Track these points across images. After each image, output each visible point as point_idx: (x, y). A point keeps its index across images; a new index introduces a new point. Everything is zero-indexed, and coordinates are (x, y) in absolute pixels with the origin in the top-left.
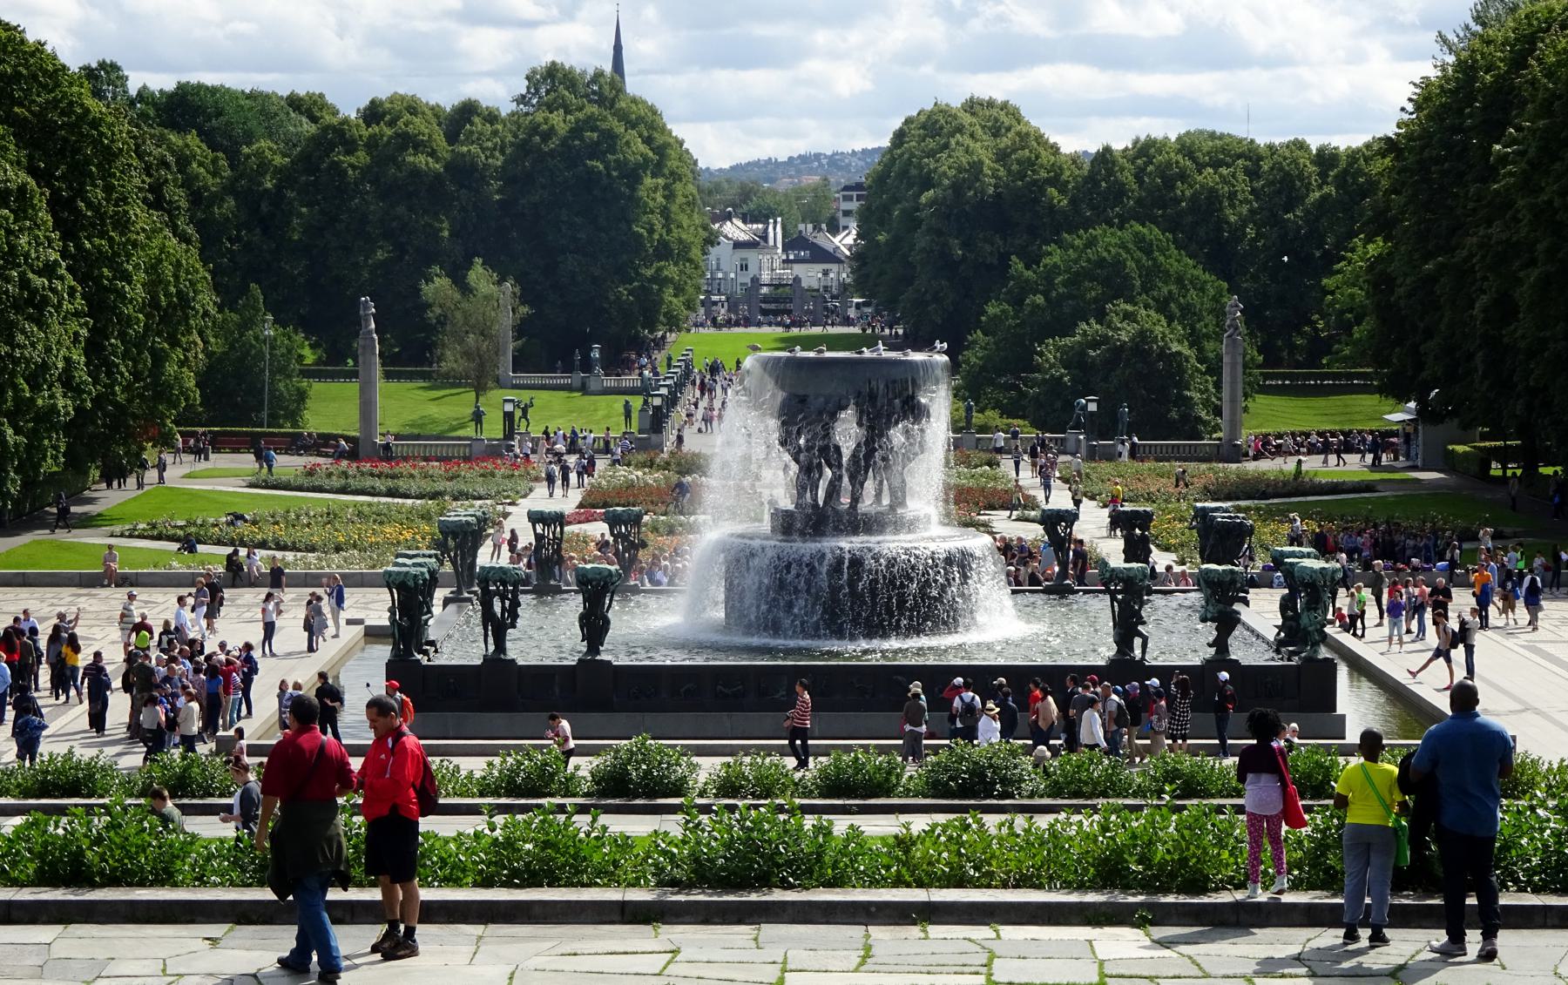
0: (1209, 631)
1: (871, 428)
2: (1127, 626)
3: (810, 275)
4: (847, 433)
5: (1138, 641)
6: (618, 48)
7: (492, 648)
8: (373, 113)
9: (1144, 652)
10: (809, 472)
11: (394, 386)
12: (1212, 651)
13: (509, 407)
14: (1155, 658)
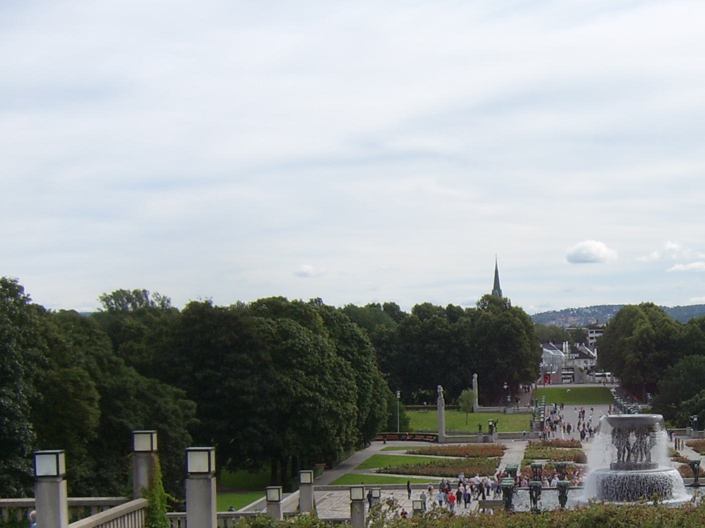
6: (496, 272)
8: (417, 309)
11: (449, 412)
13: (491, 423)
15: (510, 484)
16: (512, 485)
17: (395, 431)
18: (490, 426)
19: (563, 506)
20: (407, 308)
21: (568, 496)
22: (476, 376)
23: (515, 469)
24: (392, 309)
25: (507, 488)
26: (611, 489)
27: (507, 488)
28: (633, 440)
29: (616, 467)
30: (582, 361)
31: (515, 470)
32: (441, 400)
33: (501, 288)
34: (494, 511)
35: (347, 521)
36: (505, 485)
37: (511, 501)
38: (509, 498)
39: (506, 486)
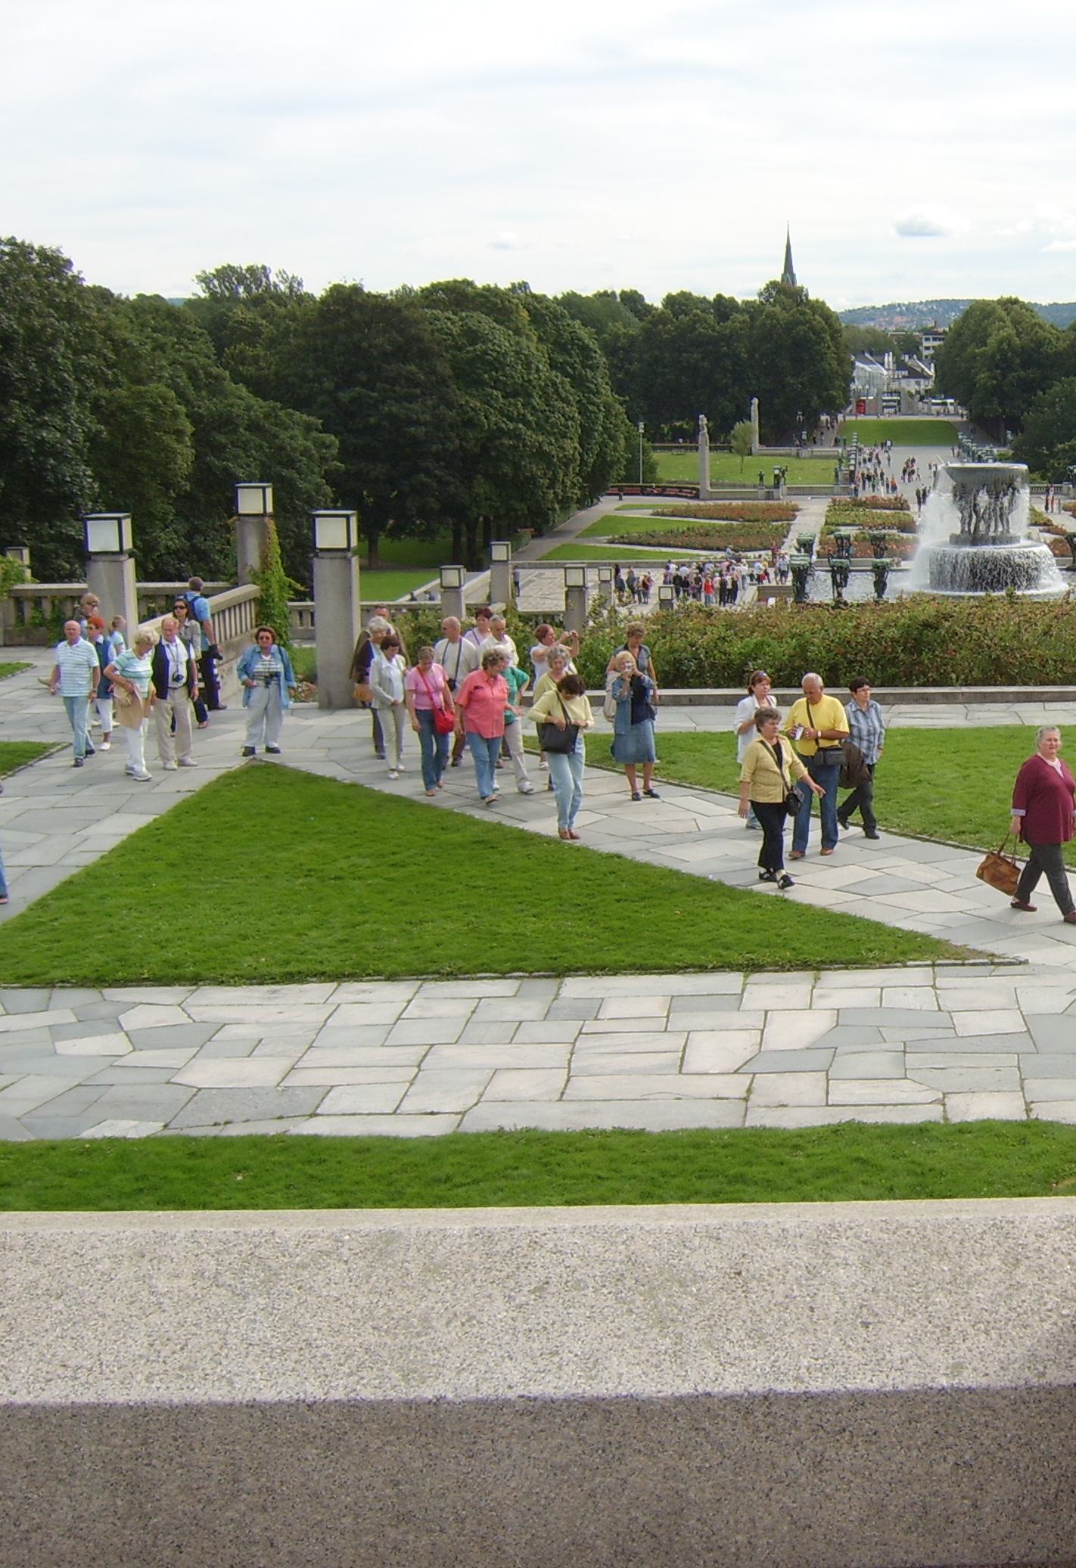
3: (911, 386)
8: (670, 301)
13: (777, 472)
17: (637, 480)
18: (776, 476)
19: (880, 596)
20: (655, 299)
22: (756, 401)
24: (632, 299)
30: (913, 381)
32: (704, 437)
33: (795, 271)
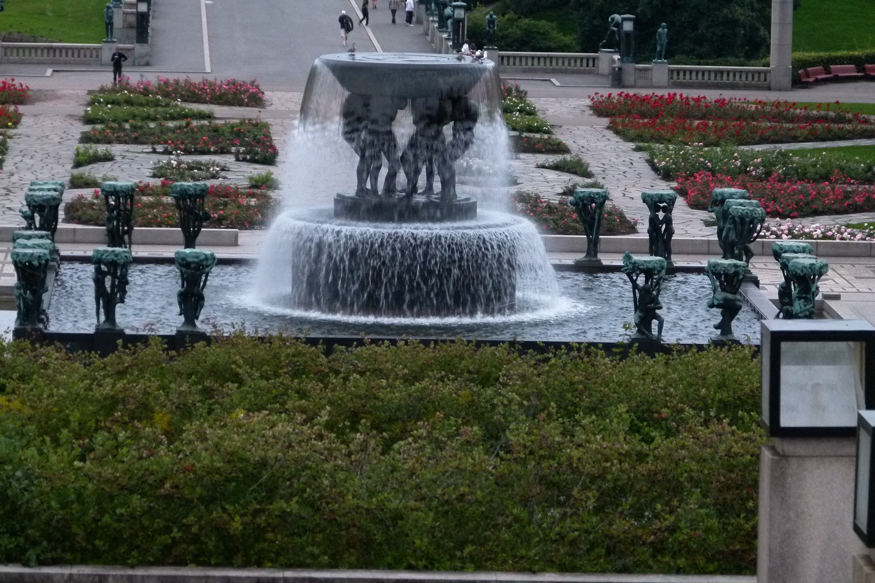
0: (717, 316)
1: (551, 209)
2: (647, 306)
4: (404, 128)
5: (655, 322)
7: (103, 318)
9: (660, 331)
10: (367, 169)
12: (719, 332)
14: (669, 337)
15: (37, 251)
16: (45, 254)
21: (206, 292)
23: (54, 199)
25: (30, 262)
26: (329, 275)
27: (30, 262)
28: (403, 135)
29: (349, 208)
31: (53, 203)
34: (155, 350)
35: (321, 341)
36: (25, 254)
37: (40, 301)
38: (33, 292)
39: (27, 259)
